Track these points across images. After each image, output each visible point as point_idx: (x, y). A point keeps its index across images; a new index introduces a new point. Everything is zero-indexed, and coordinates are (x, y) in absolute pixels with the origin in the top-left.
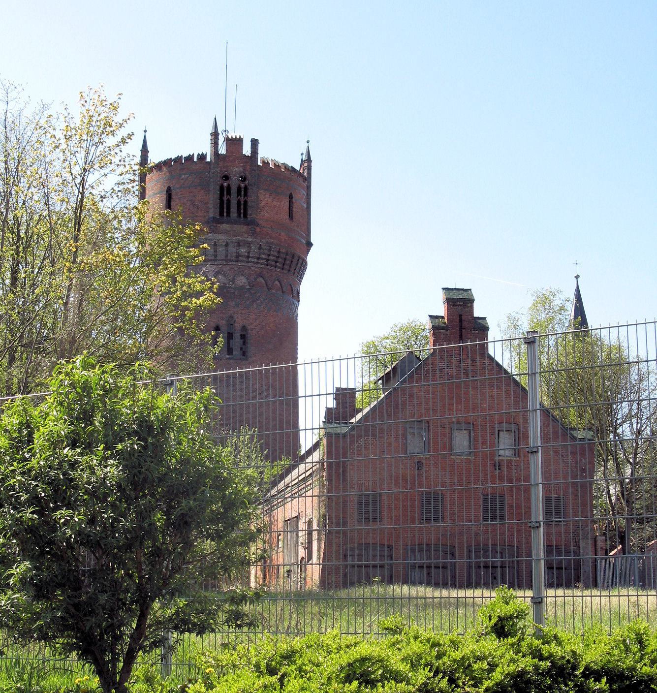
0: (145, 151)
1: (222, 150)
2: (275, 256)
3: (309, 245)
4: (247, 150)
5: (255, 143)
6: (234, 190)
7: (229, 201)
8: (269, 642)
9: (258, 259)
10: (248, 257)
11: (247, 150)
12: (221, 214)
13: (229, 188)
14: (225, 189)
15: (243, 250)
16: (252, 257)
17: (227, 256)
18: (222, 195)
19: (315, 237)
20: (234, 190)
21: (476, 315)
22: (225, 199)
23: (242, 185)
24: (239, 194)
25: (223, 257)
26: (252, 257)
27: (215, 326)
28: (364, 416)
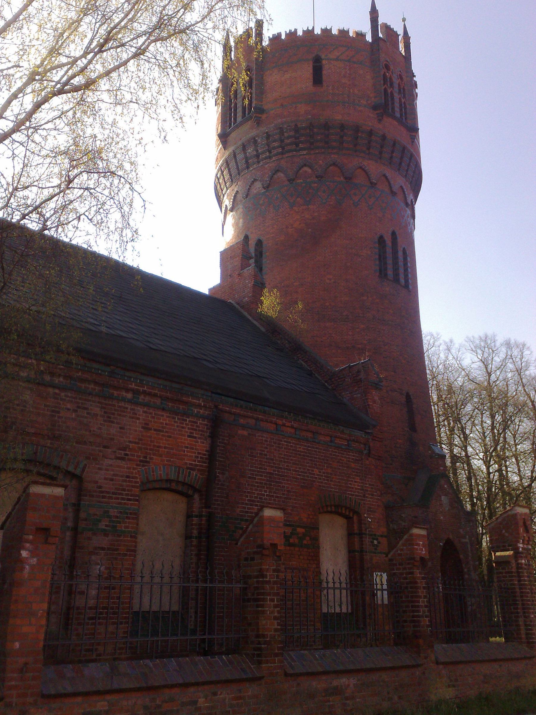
4: (252, 41)
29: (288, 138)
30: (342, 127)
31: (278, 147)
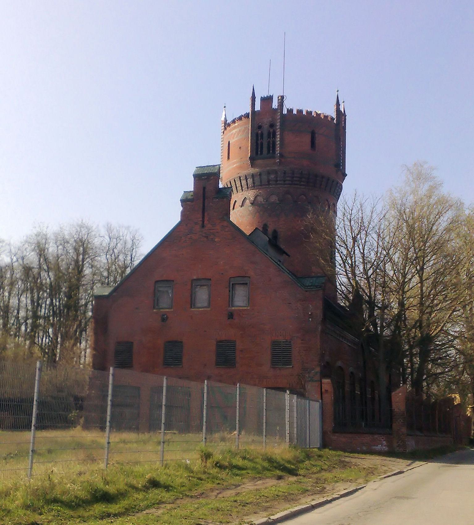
0: (225, 118)
1: (258, 107)
2: (289, 180)
3: (345, 175)
4: (275, 105)
5: (282, 99)
6: (265, 135)
7: (262, 144)
8: (446, 287)
9: (284, 181)
10: (277, 181)
11: (275, 105)
12: (257, 153)
13: (262, 134)
14: (259, 136)
15: (272, 176)
16: (280, 180)
17: (261, 182)
18: (257, 139)
19: (348, 169)
20: (265, 135)
21: (192, 190)
22: (259, 142)
23: (271, 130)
24: (269, 136)
25: (259, 184)
26: (280, 180)
27: (36, 242)
28: (35, 379)
29: (296, 177)
30: (323, 177)
31: (289, 180)
